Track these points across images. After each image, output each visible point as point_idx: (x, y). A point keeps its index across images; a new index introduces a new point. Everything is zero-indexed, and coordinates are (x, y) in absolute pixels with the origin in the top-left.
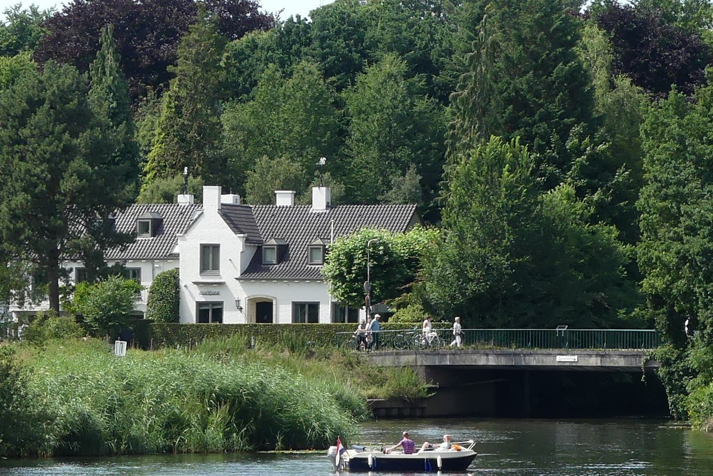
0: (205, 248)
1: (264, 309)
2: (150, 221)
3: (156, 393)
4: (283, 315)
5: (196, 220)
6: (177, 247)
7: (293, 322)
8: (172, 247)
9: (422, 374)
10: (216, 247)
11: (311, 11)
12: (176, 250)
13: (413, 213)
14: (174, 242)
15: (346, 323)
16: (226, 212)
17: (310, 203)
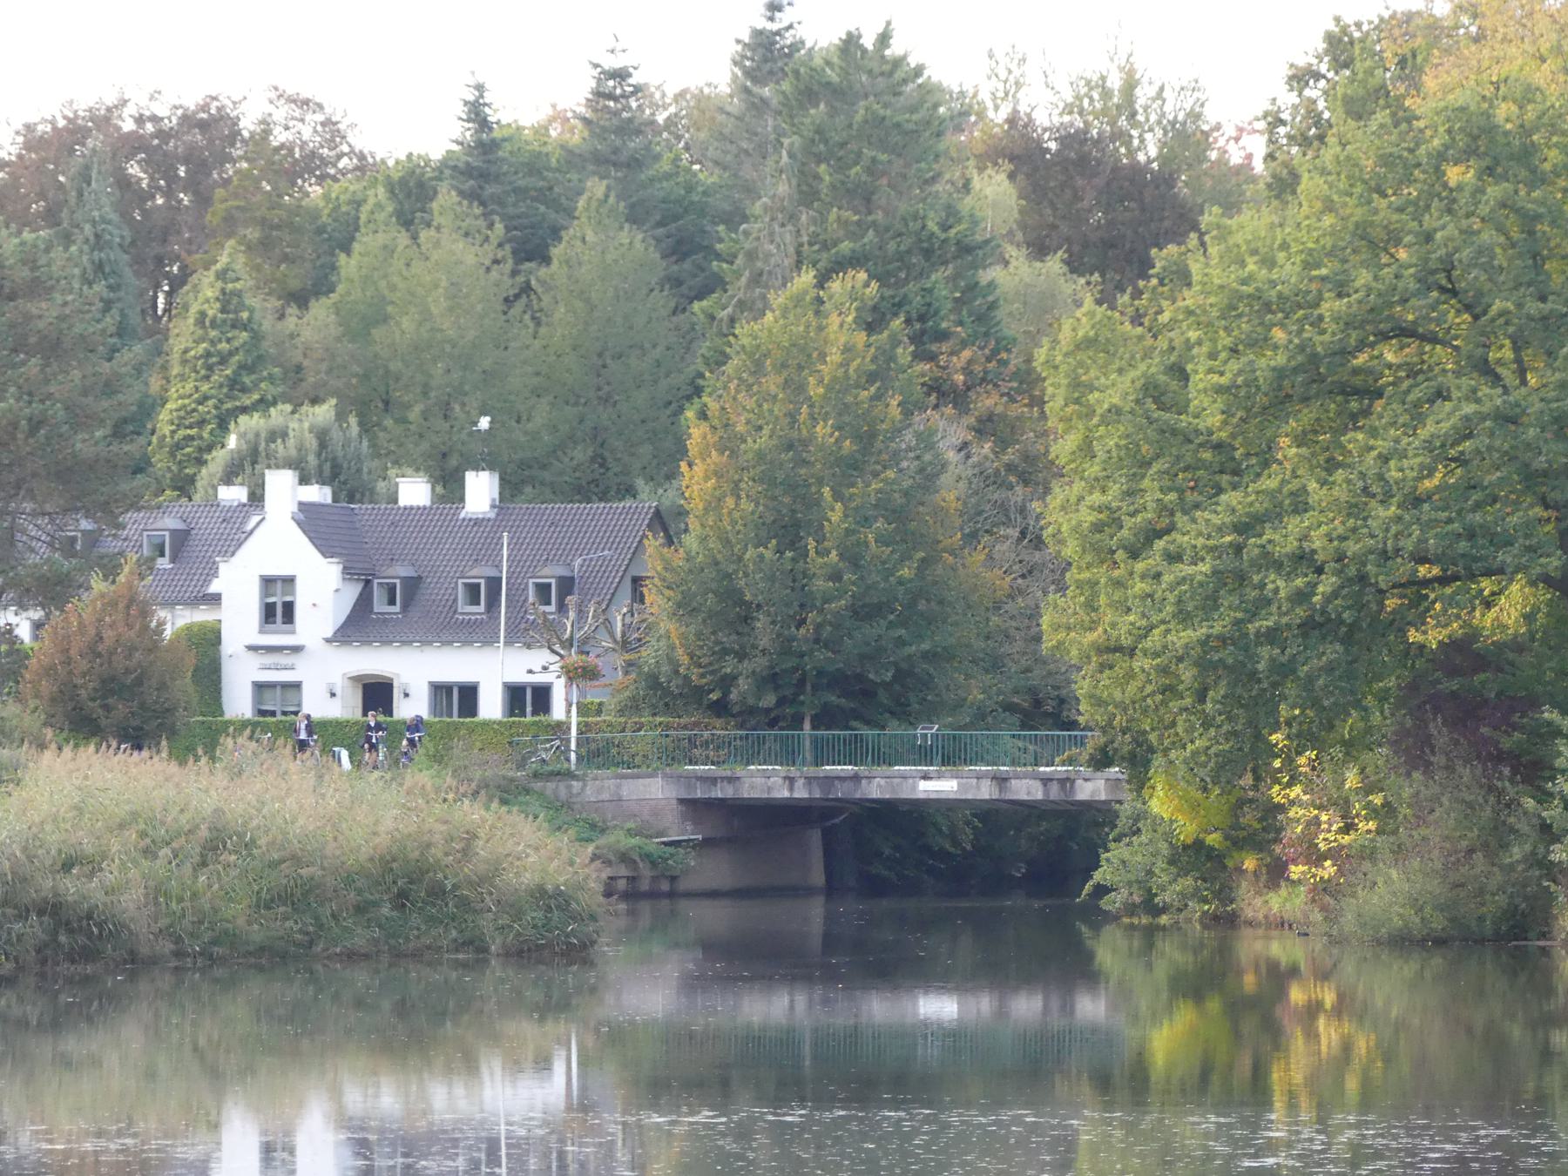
0: (268, 582)
1: (377, 693)
2: (167, 533)
3: (1314, 876)
4: (491, 706)
5: (251, 532)
6: (216, 581)
7: (504, 716)
8: (207, 582)
9: (675, 802)
10: (289, 581)
11: (1340, 47)
12: (214, 587)
13: (651, 519)
14: (213, 572)
15: (455, 718)
16: (308, 518)
17: (462, 499)
